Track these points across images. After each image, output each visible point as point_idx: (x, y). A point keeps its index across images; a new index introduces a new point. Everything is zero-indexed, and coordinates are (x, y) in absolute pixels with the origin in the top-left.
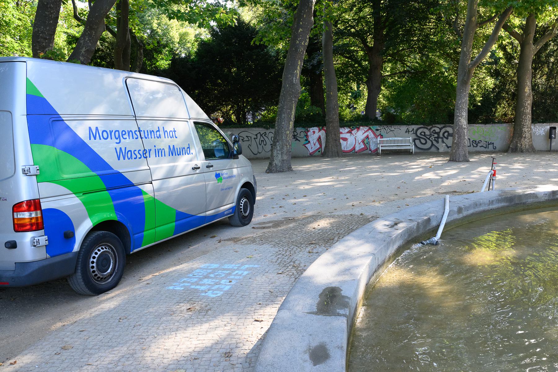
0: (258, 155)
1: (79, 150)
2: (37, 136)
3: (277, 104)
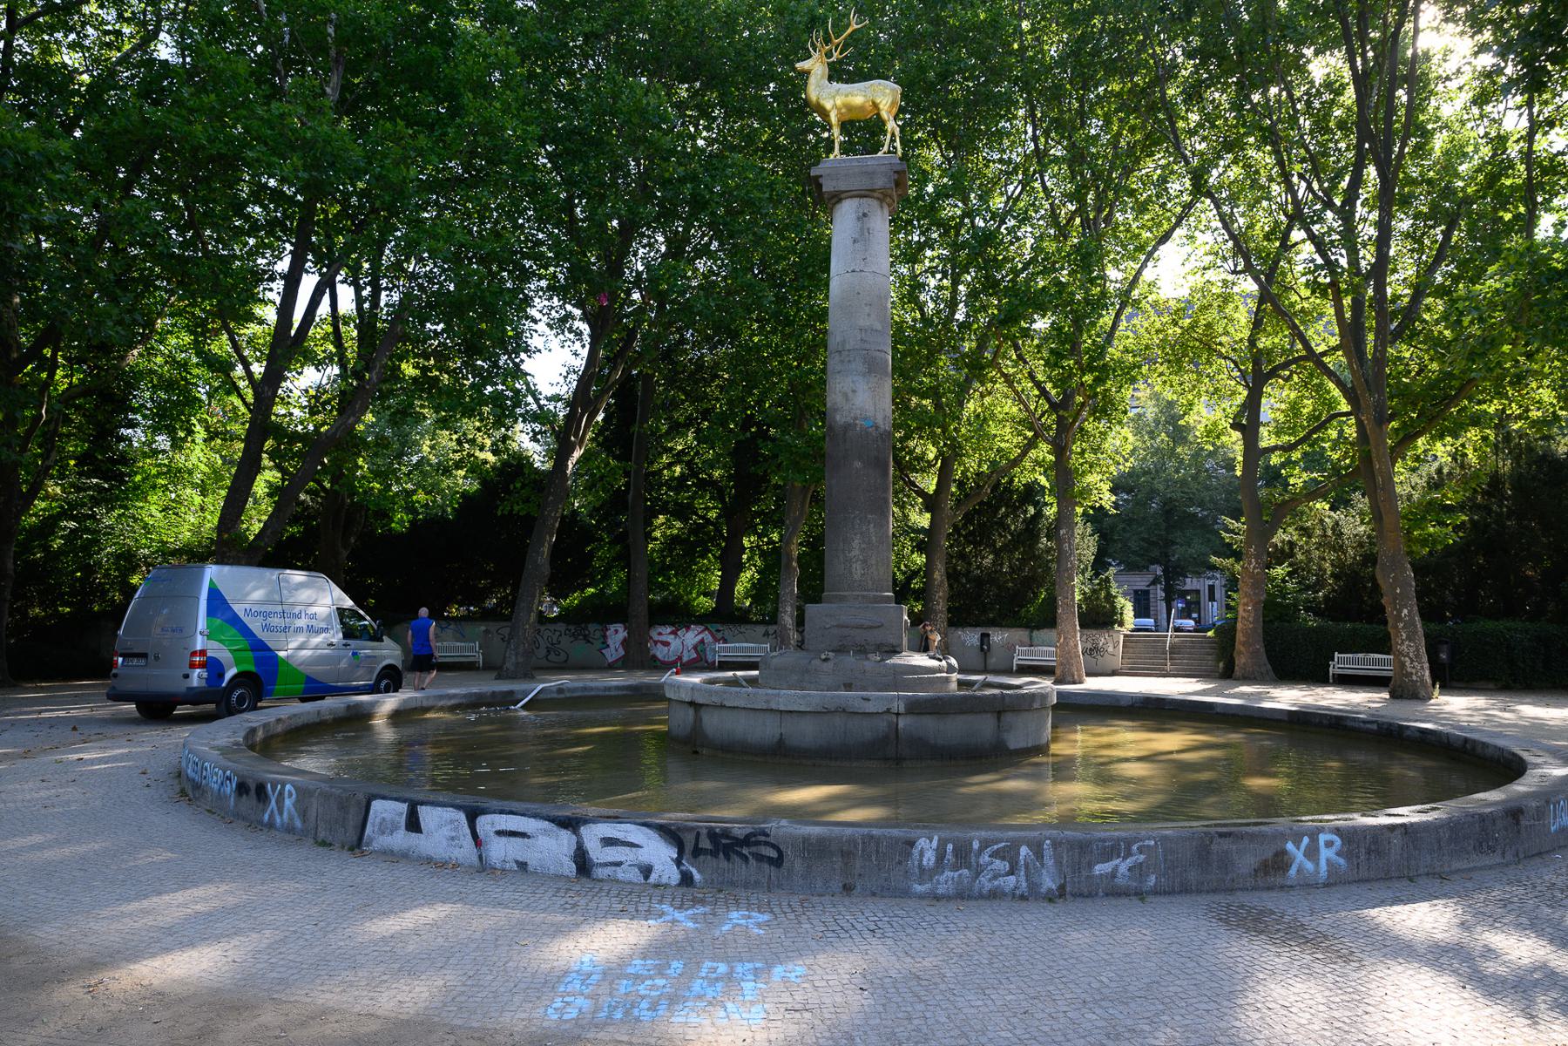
1: (235, 621)
2: (211, 612)
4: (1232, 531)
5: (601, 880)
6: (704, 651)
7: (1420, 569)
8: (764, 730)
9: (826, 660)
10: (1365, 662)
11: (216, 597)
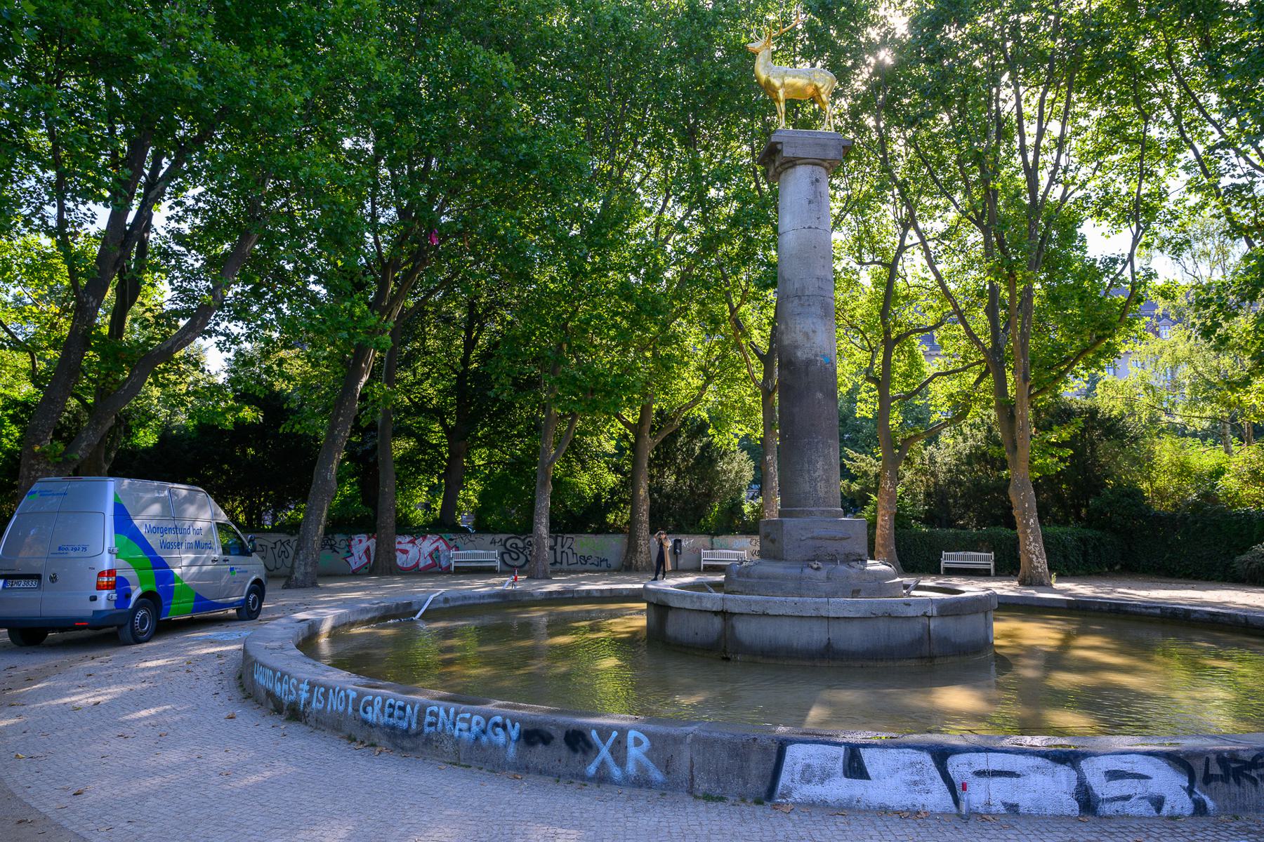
0: (275, 572)
2: (119, 529)
3: (304, 501)
4: (852, 459)
5: (1109, 817)
6: (438, 557)
7: (1036, 486)
8: (815, 635)
9: (818, 569)
10: (964, 558)
11: (120, 510)
